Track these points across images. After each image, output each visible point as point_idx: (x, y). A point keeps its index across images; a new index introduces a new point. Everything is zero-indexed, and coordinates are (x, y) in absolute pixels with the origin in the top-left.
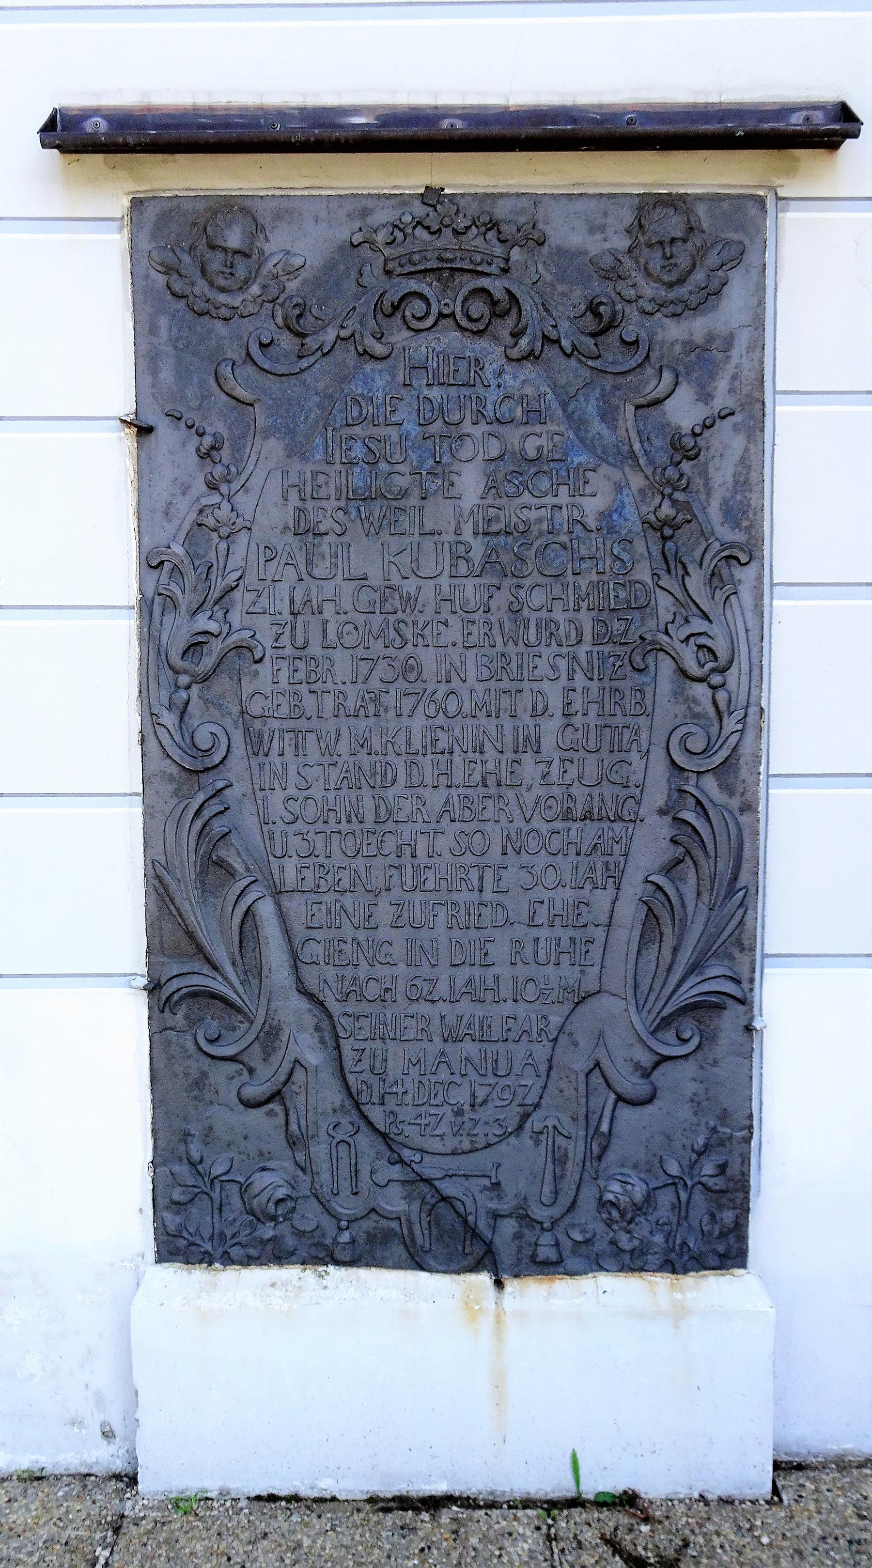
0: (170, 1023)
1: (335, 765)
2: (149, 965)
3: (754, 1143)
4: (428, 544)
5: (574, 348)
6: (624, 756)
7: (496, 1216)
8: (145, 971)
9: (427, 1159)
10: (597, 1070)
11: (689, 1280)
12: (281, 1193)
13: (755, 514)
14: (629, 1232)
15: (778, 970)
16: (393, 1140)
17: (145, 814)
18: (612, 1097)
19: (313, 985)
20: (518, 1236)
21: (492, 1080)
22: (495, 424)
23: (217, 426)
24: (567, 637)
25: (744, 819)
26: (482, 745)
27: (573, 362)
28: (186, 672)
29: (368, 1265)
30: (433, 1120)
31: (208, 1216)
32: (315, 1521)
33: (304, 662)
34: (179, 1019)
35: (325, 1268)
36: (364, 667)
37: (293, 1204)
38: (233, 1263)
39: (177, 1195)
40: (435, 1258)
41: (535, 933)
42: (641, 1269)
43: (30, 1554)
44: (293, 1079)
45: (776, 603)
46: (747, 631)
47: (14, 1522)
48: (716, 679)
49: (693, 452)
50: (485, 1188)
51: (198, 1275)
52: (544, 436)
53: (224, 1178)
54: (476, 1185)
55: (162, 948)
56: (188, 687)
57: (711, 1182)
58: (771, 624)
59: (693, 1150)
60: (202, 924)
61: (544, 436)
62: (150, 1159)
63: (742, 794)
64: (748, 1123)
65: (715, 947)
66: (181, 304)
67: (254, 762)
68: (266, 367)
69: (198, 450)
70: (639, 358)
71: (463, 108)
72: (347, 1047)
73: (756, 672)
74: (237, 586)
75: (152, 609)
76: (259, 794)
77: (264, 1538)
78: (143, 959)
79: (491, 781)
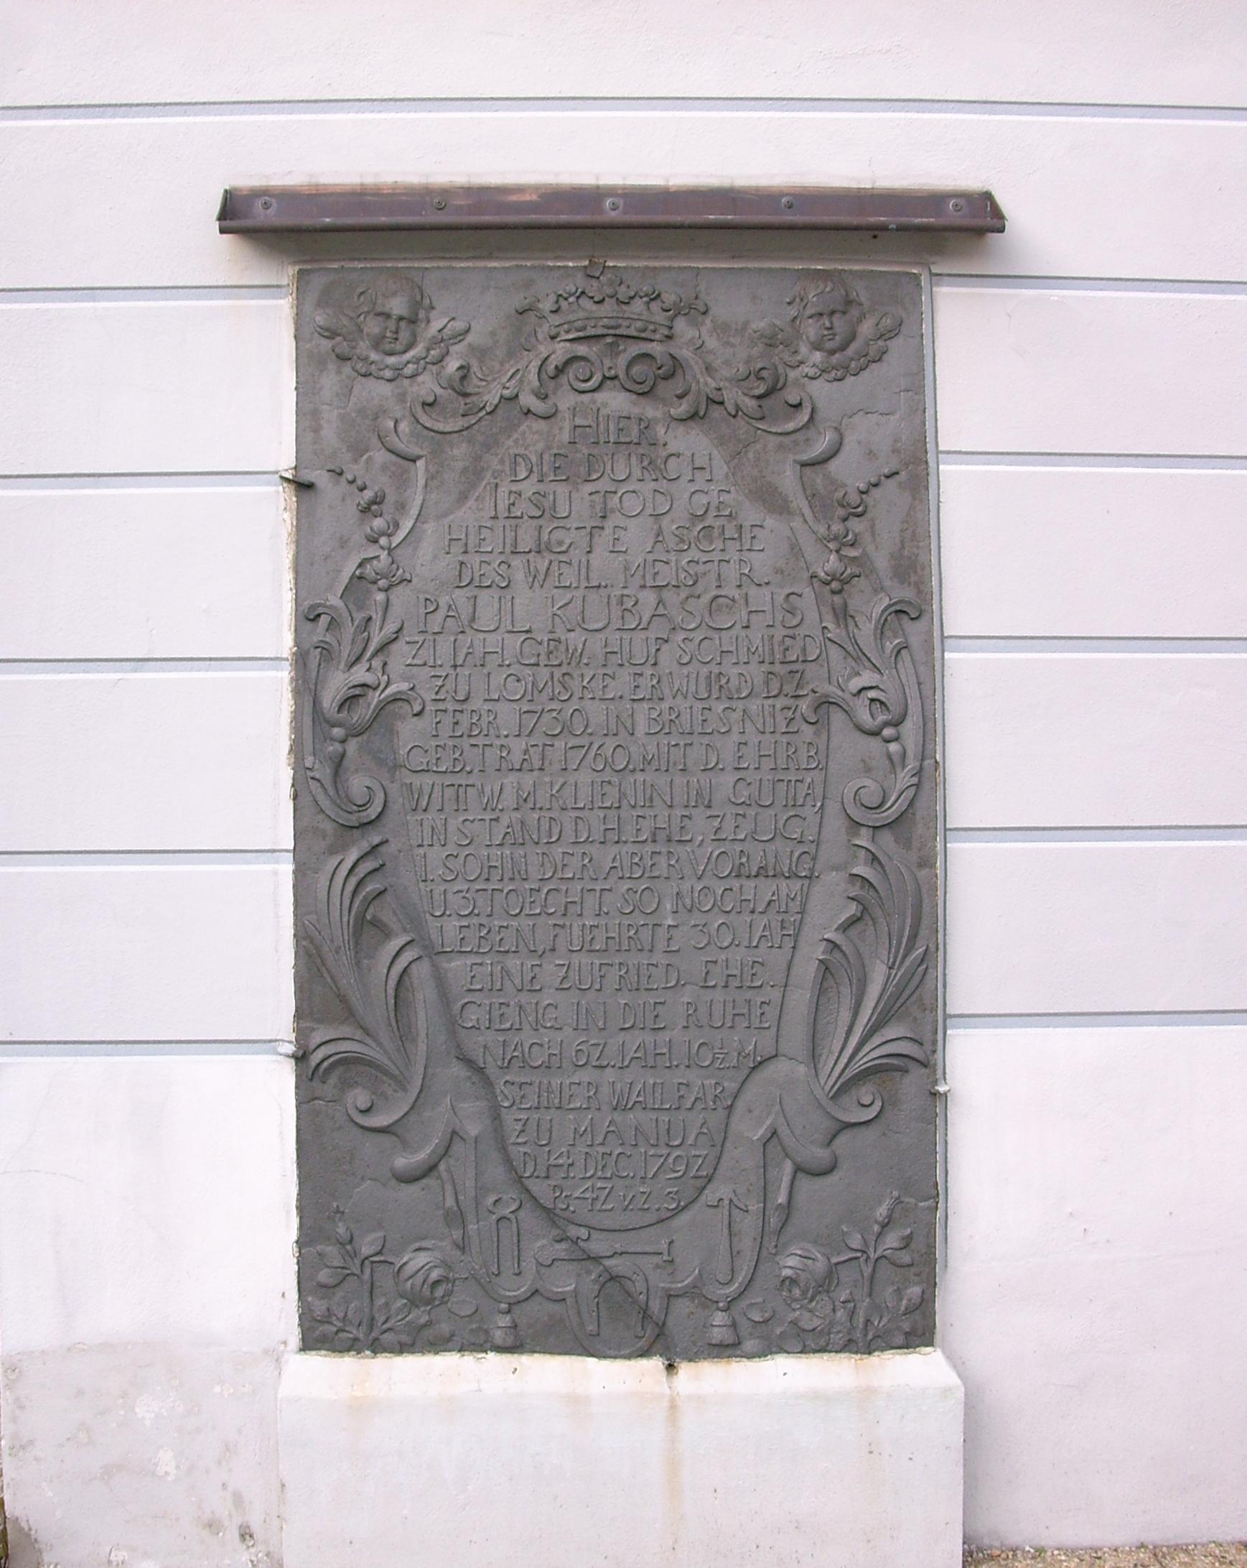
0: (318, 1094)
1: (497, 820)
4: (593, 596)
5: (738, 408)
6: (798, 811)
7: (670, 1296)
8: (293, 1037)
9: (595, 1235)
11: (875, 1359)
12: (435, 1275)
13: (923, 569)
15: (961, 1031)
18: (788, 1167)
21: (665, 1151)
23: (379, 482)
24: (739, 690)
25: (923, 873)
28: (340, 725)
36: (530, 721)
38: (385, 1350)
41: (707, 996)
44: (451, 1152)
45: (947, 655)
46: (919, 684)
48: (887, 732)
49: (860, 509)
50: (657, 1266)
51: (348, 1363)
54: (648, 1263)
55: (312, 1013)
56: (343, 741)
64: (933, 1192)
68: (428, 425)
70: (804, 417)
72: (508, 1117)
73: (930, 725)
75: (309, 665)
79: (661, 836)
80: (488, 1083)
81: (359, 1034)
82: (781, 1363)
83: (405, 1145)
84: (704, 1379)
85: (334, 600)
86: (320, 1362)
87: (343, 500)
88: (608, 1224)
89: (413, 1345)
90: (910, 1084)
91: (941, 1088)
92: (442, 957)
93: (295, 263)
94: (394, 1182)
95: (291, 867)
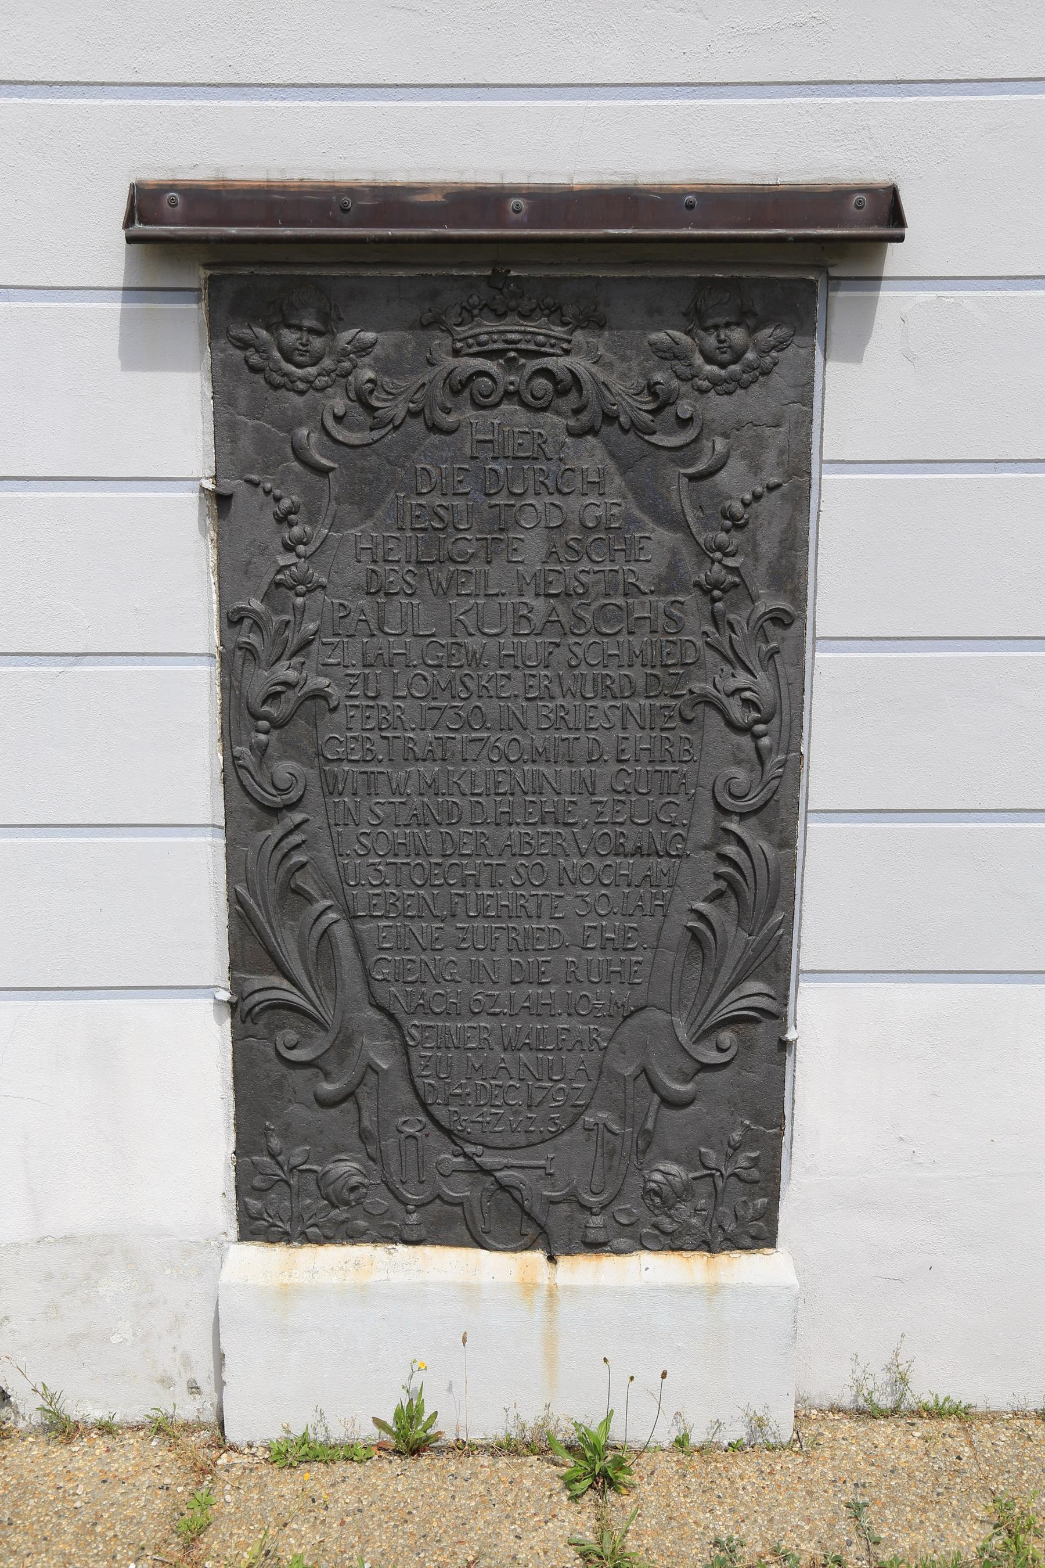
2: (232, 979)
3: (785, 1140)
9: (487, 1151)
10: (643, 1076)
11: (723, 1259)
12: (356, 1179)
14: (670, 1216)
16: (455, 1135)
17: (227, 845)
19: (383, 998)
20: (570, 1218)
22: (556, 495)
26: (541, 787)
27: (631, 435)
29: (433, 1244)
30: (494, 1119)
31: (284, 1193)
32: (387, 1466)
33: (376, 710)
34: (260, 1028)
35: (394, 1246)
37: (364, 1190)
39: (258, 1181)
40: (495, 1238)
42: (680, 1249)
43: (138, 1499)
45: (818, 655)
47: (117, 1470)
51: (279, 1253)
52: (603, 507)
53: (303, 1167)
55: (244, 966)
57: (744, 1174)
58: (812, 675)
59: (729, 1145)
60: (282, 945)
61: (603, 507)
62: (232, 1148)
63: (781, 832)
65: (753, 968)
66: (259, 378)
67: (330, 800)
69: (275, 514)
71: (528, 188)
72: (414, 1054)
74: (313, 639)
75: (235, 659)
76: (334, 829)
77: (344, 1481)
78: (227, 975)
80: (399, 1026)
81: (286, 985)
82: (646, 1258)
83: (327, 1076)
84: (580, 1271)
85: (256, 604)
86: (255, 1252)
87: (261, 509)
88: (498, 1142)
89: (332, 1238)
90: (762, 1031)
91: (790, 1035)
92: (358, 921)
93: (206, 266)
94: (316, 1106)
95: (224, 842)
